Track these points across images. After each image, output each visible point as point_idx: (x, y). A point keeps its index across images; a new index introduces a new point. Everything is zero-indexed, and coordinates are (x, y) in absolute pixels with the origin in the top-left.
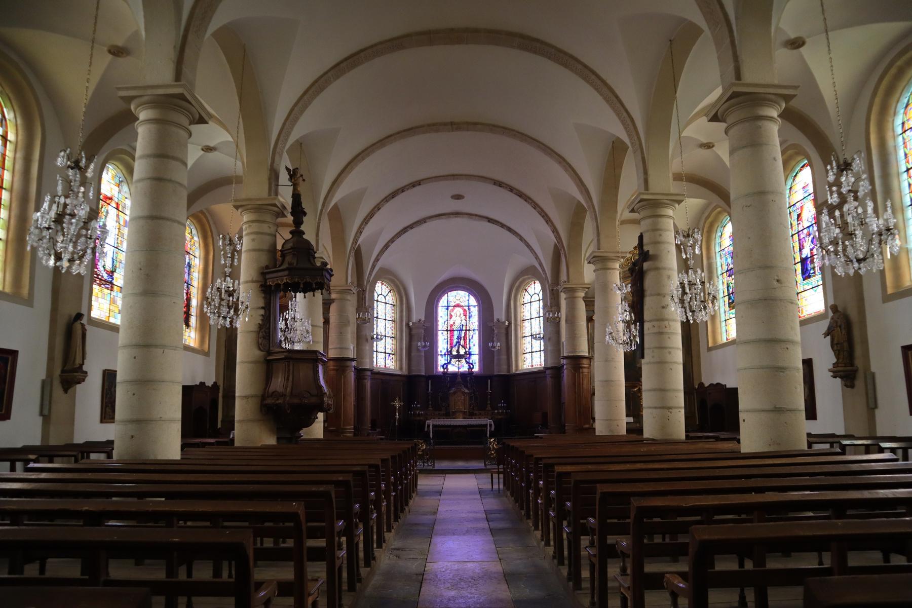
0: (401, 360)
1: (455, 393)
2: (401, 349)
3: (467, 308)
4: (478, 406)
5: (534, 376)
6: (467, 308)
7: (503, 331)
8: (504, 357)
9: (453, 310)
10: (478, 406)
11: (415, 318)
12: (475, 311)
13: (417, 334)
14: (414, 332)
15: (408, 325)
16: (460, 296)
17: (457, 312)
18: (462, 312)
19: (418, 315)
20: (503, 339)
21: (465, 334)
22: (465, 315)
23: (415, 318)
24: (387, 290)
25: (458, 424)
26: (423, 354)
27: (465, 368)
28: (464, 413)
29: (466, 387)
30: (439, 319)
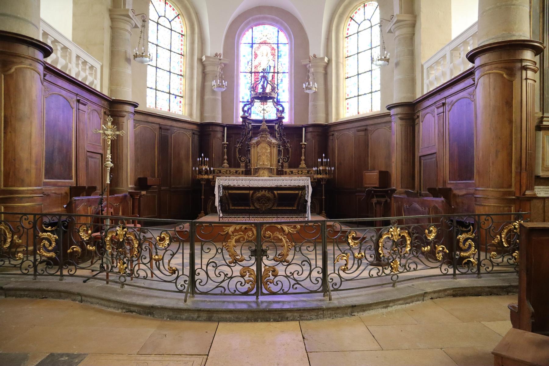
0: (191, 105)
1: (258, 143)
2: (191, 90)
3: (275, 46)
4: (290, 160)
5: (364, 125)
7: (321, 70)
8: (321, 103)
9: (258, 48)
10: (290, 160)
11: (210, 51)
12: (285, 50)
13: (212, 72)
14: (208, 69)
15: (200, 60)
16: (267, 32)
17: (264, 51)
19: (214, 47)
20: (322, 81)
21: (273, 77)
22: (273, 55)
23: (210, 51)
24: (176, 12)
26: (220, 98)
27: (272, 115)
28: (270, 170)
29: (274, 137)
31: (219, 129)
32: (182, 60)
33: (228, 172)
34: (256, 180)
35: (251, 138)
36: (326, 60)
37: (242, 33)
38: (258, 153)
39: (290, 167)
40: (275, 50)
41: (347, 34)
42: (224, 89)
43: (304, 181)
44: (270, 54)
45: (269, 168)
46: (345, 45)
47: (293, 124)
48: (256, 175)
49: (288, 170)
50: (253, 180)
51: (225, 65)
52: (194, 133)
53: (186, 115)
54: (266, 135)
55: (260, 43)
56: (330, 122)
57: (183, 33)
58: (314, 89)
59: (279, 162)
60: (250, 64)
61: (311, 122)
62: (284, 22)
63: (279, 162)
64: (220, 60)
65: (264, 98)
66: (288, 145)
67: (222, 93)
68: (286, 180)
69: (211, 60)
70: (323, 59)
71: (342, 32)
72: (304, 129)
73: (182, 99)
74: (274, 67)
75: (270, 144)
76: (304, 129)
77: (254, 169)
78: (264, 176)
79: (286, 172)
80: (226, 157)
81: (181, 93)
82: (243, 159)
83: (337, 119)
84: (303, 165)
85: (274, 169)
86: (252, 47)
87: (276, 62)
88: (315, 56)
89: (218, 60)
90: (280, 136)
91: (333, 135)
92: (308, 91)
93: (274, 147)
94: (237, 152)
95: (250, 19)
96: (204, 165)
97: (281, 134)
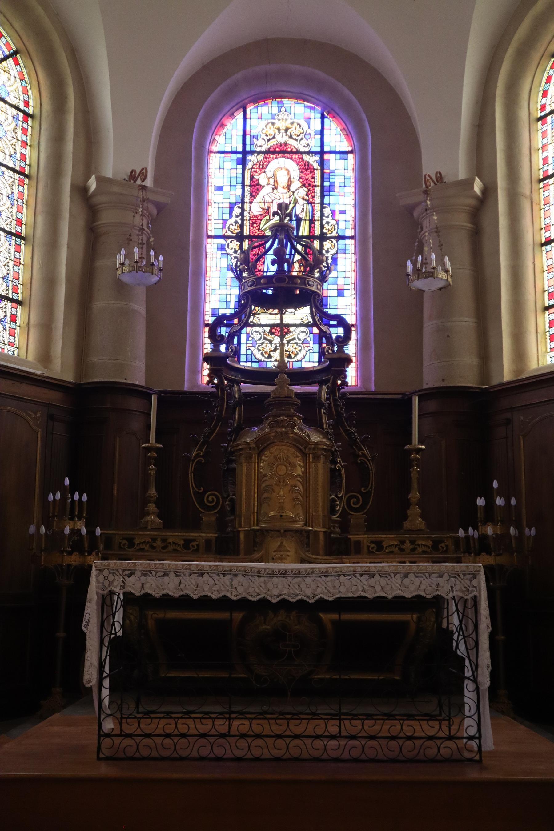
1: (262, 445)
2: (50, 282)
3: (313, 161)
6: (313, 161)
7: (462, 220)
8: (464, 322)
9: (262, 166)
11: (113, 163)
14: (107, 218)
15: (80, 191)
16: (287, 119)
17: (279, 163)
18: (295, 172)
19: (128, 149)
20: (463, 250)
22: (308, 184)
23: (112, 164)
25: (277, 590)
26: (140, 308)
30: (213, 195)
31: (134, 403)
32: (25, 190)
33: (159, 543)
34: (258, 573)
35: (238, 431)
36: (477, 186)
37: (213, 122)
38: (261, 477)
39: (371, 527)
40: (313, 170)
41: (543, 107)
42: (155, 279)
43: (458, 583)
44: (297, 184)
45: (299, 532)
46: (539, 142)
47: (373, 388)
48: (256, 555)
49: (363, 537)
50: (244, 572)
51: (160, 207)
52: (51, 417)
53: (30, 358)
54: (291, 416)
55: (268, 152)
56: (495, 382)
57: (30, 110)
58: (443, 276)
59: (333, 511)
60: (237, 211)
61: (430, 379)
62: (340, 86)
63: (333, 511)
64: (144, 188)
65: (286, 292)
66: (366, 451)
67: (151, 290)
68: (384, 574)
69: (116, 189)
70: (468, 183)
71: (525, 104)
72: (416, 400)
73: (19, 311)
74: (312, 221)
75: (303, 447)
76: (416, 400)
77: (248, 533)
78: (281, 559)
79: (358, 543)
80: (153, 492)
81: (15, 290)
82: (210, 498)
83: (518, 370)
84: (415, 520)
85: (316, 533)
86: (243, 162)
87: (318, 207)
88: (439, 178)
89: (135, 192)
90: (334, 427)
91: (509, 422)
92: (419, 284)
93: (316, 458)
94: (191, 476)
95: (239, 76)
96: (72, 519)
97: (339, 414)
